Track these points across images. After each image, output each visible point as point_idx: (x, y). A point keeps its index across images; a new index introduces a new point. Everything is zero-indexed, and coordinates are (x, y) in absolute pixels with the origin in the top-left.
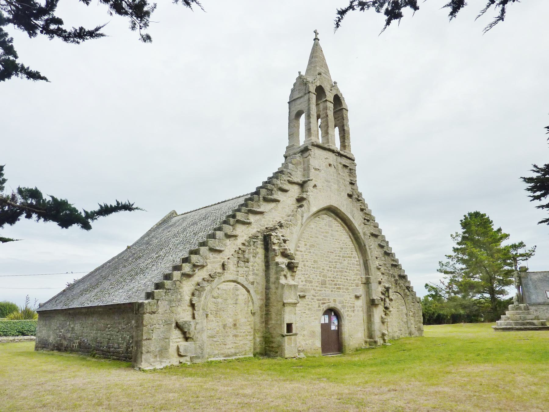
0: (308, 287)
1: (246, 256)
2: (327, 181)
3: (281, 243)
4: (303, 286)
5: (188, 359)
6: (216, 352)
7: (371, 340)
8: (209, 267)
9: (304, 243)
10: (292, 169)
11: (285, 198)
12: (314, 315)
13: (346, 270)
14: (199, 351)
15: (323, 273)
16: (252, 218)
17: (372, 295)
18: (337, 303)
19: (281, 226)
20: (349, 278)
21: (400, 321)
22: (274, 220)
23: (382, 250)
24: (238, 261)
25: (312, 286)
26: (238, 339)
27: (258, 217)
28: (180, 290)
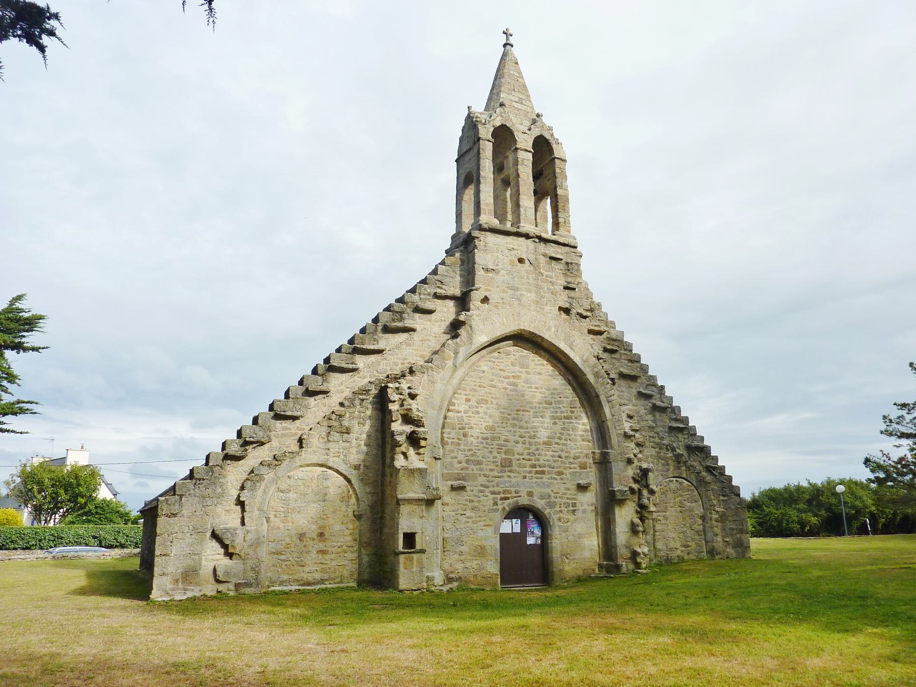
0: (473, 472)
1: (346, 423)
2: (513, 288)
3: (404, 400)
4: (462, 469)
5: (232, 587)
6: (286, 577)
7: (611, 563)
8: (275, 443)
9: (465, 397)
10: (446, 274)
11: (428, 323)
12: (484, 518)
13: (558, 441)
14: (251, 574)
15: (506, 448)
16: (361, 361)
17: (611, 483)
18: (535, 498)
19: (411, 372)
20: (563, 454)
21: (685, 529)
22: (406, 361)
23: (647, 402)
24: (329, 433)
25: (481, 470)
26: (328, 557)
27: (372, 358)
28: (221, 480)
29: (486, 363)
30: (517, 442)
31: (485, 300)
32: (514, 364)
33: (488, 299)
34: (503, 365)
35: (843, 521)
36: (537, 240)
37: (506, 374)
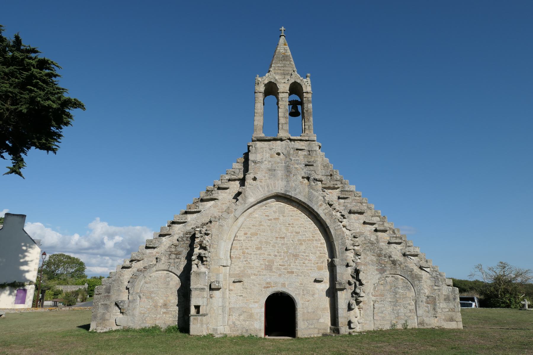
16: (189, 217)
29: (258, 212)
31: (255, 179)
33: (256, 179)
34: (268, 213)
35: (463, 308)
36: (289, 141)
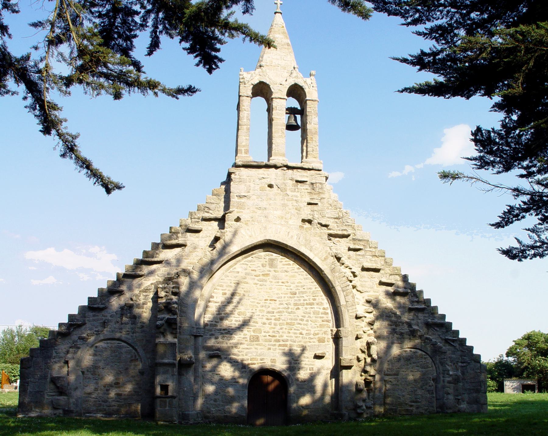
13: (300, 322)
15: (255, 328)
20: (304, 332)
30: (264, 324)
31: (238, 219)
32: (264, 265)
34: (255, 266)
36: (285, 168)
37: (257, 273)
